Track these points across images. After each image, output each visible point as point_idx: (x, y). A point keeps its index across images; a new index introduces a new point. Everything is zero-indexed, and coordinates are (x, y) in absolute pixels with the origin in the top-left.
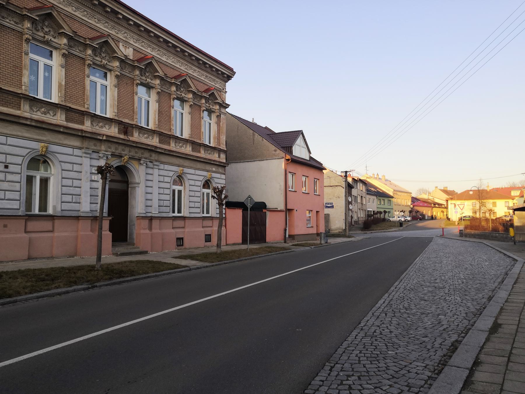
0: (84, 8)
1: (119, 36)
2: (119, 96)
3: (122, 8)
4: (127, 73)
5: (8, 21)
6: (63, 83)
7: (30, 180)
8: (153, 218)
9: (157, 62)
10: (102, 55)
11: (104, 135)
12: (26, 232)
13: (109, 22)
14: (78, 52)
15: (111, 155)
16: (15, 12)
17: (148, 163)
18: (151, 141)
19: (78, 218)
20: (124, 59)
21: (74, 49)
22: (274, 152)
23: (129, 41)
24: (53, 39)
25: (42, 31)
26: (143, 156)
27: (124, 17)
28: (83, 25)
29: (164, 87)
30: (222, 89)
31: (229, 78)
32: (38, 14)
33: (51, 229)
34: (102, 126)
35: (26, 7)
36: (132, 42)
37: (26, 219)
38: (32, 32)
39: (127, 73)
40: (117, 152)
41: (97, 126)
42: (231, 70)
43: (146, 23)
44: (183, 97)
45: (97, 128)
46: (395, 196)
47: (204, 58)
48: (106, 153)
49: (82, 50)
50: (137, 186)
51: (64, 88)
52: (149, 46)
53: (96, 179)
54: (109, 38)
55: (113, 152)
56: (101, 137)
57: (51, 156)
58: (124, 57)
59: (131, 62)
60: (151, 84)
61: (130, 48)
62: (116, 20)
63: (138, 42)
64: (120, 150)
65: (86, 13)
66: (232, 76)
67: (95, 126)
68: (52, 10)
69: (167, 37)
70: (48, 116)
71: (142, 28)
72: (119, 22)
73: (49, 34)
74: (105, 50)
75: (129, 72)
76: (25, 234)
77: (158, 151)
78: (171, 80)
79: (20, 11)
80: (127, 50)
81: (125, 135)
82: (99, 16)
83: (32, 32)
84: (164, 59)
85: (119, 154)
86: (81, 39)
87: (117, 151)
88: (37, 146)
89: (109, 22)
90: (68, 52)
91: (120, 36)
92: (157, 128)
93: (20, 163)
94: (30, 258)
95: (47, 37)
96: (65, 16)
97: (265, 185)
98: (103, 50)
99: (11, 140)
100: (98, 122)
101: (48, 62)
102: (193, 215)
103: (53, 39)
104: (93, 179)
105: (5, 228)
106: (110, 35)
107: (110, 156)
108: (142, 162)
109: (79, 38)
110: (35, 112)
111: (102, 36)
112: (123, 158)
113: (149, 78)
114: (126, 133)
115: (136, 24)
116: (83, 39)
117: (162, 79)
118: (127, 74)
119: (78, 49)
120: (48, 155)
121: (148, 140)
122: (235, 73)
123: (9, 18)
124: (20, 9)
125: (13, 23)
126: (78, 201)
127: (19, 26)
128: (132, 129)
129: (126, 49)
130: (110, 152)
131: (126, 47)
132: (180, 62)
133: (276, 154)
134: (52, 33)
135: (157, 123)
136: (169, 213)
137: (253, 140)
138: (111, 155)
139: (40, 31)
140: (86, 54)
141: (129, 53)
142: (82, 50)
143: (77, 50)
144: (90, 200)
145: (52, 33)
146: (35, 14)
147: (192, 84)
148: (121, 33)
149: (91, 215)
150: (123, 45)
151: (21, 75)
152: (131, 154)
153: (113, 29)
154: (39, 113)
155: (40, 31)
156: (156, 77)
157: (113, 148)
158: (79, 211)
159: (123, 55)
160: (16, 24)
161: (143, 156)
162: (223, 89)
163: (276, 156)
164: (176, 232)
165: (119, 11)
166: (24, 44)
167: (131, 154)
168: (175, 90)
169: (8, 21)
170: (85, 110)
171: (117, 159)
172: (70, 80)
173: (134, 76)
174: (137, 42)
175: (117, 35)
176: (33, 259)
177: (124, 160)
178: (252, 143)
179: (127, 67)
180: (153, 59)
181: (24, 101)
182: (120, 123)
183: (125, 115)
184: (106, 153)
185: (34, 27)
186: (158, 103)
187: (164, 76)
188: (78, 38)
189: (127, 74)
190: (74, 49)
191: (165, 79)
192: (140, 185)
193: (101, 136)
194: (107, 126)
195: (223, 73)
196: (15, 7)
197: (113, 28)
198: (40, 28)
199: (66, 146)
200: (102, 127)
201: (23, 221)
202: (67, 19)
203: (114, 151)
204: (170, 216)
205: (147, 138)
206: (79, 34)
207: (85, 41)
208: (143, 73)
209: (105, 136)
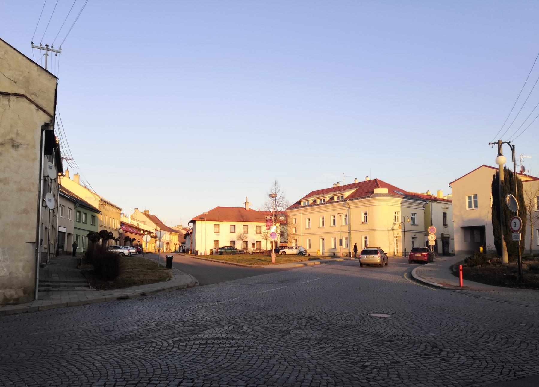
46: (101, 210)
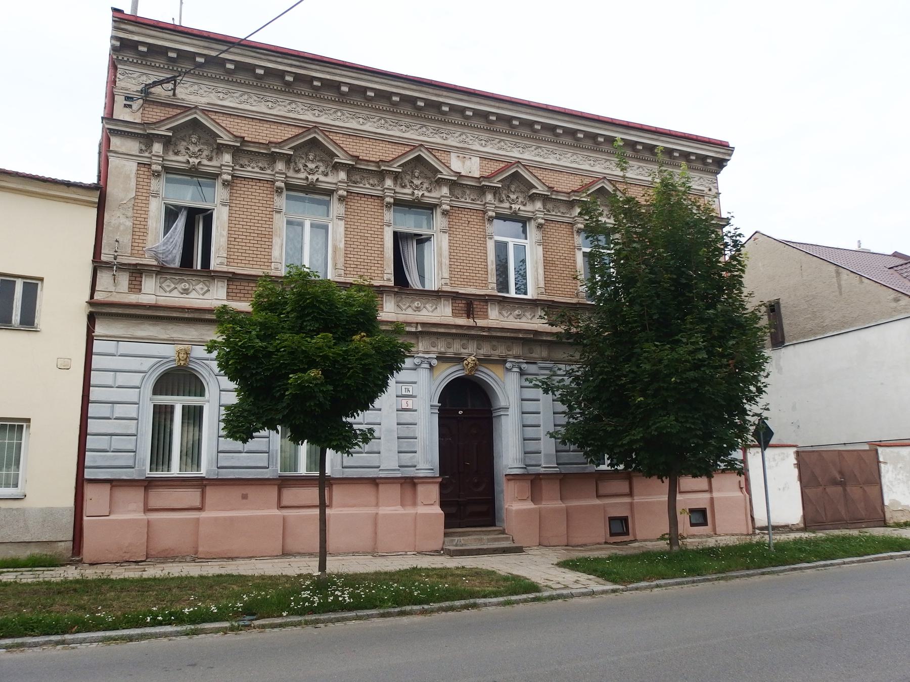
0: (498, 137)
1: (449, 142)
2: (545, 261)
3: (445, 93)
4: (467, 203)
5: (249, 169)
6: (342, 245)
7: (162, 415)
8: (416, 481)
9: (527, 169)
10: (415, 182)
11: (417, 323)
12: (281, 507)
13: (428, 124)
14: (257, 173)
15: (438, 358)
16: (259, 153)
17: (524, 366)
18: (530, 321)
19: (374, 482)
20: (455, 178)
21: (361, 185)
22: (894, 305)
23: (470, 147)
24: (522, 208)
25: (305, 170)
26: (510, 353)
27: (453, 108)
28: (377, 141)
29: (554, 213)
30: (706, 190)
31: (720, 164)
32: (500, 178)
33: (197, 504)
34: (519, 315)
35: (272, 140)
36: (476, 147)
37: (560, 480)
38: (284, 176)
39: (467, 203)
40: (451, 351)
41: (410, 309)
42: (723, 145)
43: (497, 104)
44: (515, 212)
45: (410, 311)
47: (404, 88)
48: (427, 356)
49: (376, 182)
50: (502, 413)
51: (342, 253)
52: (516, 145)
53: (410, 407)
54: (421, 151)
55: (440, 353)
56: (412, 327)
57: (202, 370)
58: (455, 176)
59: (472, 181)
60: (522, 214)
61: (473, 158)
62: (440, 117)
63: (491, 144)
64: (456, 348)
65: (383, 122)
66: (727, 158)
67: (507, 317)
68: (315, 132)
69: (499, 108)
70: (524, 320)
71: (492, 116)
72: (447, 118)
73: (422, 187)
74: (421, 172)
75: (472, 200)
76: (278, 511)
77: (544, 338)
78: (569, 197)
79: (265, 149)
80: (468, 163)
81: (468, 317)
82: (408, 120)
83: (284, 176)
84: (551, 160)
85: (455, 354)
86: (371, 166)
87: (451, 350)
88: (169, 351)
89: (428, 124)
90: (347, 192)
91: (452, 141)
92: (542, 293)
93: (138, 384)
94: (285, 554)
95: (513, 206)
96: (345, 136)
97: (882, 384)
98: (416, 174)
99: (125, 347)
100: (411, 302)
101: (521, 241)
102: (350, 473)
103: (522, 208)
104: (404, 406)
105: (244, 501)
106: (520, 161)
107: (434, 362)
108: (508, 365)
109: (368, 165)
110: (506, 318)
111: (510, 165)
112: (465, 362)
113: (604, 215)
114: (469, 313)
115: (477, 113)
116: (373, 164)
117: (545, 199)
118: (467, 205)
119: (369, 183)
120: (192, 366)
121: (521, 321)
122: (732, 149)
123: (251, 165)
124: (265, 146)
125: (369, 187)
126: (376, 450)
127: (477, 202)
128: (485, 304)
129: (464, 162)
130: (434, 352)
131: (465, 157)
132: (591, 158)
133: (899, 308)
134: (322, 169)
135: (542, 284)
136: (133, 468)
137: (840, 286)
138: (438, 358)
139: (505, 201)
140: (573, 216)
141: (471, 167)
142: (565, 211)
143: (367, 186)
144: (399, 447)
145: (322, 169)
146: (286, 148)
147: (535, 179)
148: (453, 137)
149: (399, 475)
150: (459, 157)
151: (270, 247)
152: (481, 352)
153: (436, 134)
154: (511, 318)
155: (505, 201)
156: (533, 198)
157: (441, 347)
158: (378, 467)
159: (452, 174)
160: (263, 170)
161: (510, 353)
162: (710, 190)
163: (900, 312)
164: (540, 508)
165: (441, 100)
166: (576, 236)
167: (481, 352)
168: (542, 207)
169: (249, 169)
170: (381, 284)
171: (454, 366)
172: (355, 237)
173: (573, 218)
174: (489, 143)
175: (445, 142)
176: (289, 555)
177: (467, 365)
178: (837, 293)
179: (468, 192)
180: (520, 165)
181: (386, 295)
182: (454, 297)
183: (468, 280)
184: (427, 356)
185: (497, 198)
186: (541, 248)
187: (548, 191)
188: (365, 165)
189: (469, 206)
190: (361, 185)
191: (553, 197)
192: (510, 412)
193: (412, 325)
194: (528, 314)
195: (703, 159)
196: (257, 145)
197: (437, 132)
198: (505, 198)
199: (104, 339)
200: (418, 309)
201: (276, 488)
202: (220, 119)
203: (443, 350)
204: (587, 471)
205: (519, 317)
206: (365, 158)
207: (379, 167)
208: (503, 196)
209: (419, 326)
